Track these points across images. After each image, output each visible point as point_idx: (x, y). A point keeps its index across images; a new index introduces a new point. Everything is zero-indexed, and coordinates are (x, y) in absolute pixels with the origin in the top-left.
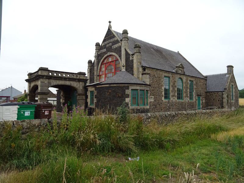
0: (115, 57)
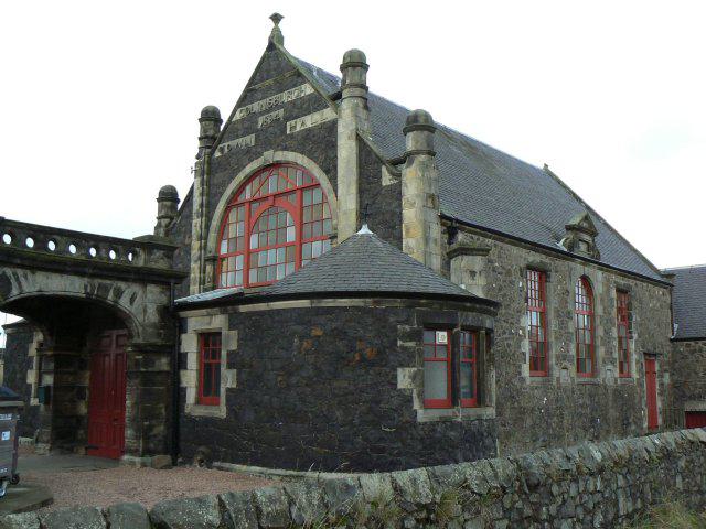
0: (299, 173)
